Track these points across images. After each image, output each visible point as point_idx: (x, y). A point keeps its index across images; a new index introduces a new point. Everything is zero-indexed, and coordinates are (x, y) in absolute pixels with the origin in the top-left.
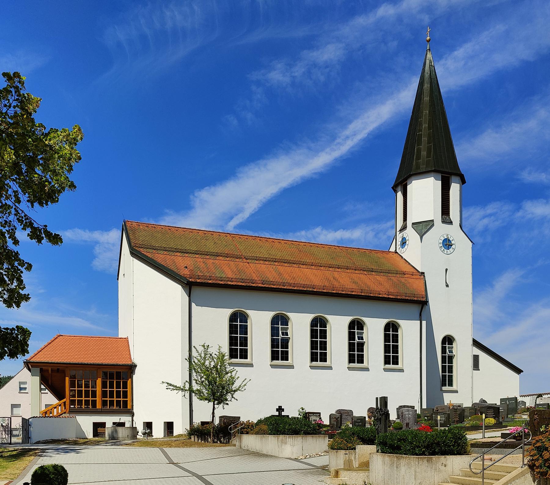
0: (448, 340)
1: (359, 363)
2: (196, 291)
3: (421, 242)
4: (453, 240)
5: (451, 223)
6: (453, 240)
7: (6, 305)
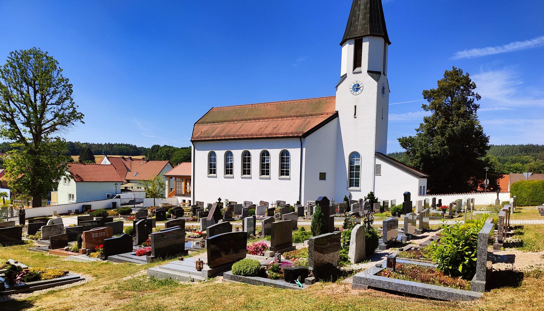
0: (355, 155)
2: (197, 144)
6: (361, 84)
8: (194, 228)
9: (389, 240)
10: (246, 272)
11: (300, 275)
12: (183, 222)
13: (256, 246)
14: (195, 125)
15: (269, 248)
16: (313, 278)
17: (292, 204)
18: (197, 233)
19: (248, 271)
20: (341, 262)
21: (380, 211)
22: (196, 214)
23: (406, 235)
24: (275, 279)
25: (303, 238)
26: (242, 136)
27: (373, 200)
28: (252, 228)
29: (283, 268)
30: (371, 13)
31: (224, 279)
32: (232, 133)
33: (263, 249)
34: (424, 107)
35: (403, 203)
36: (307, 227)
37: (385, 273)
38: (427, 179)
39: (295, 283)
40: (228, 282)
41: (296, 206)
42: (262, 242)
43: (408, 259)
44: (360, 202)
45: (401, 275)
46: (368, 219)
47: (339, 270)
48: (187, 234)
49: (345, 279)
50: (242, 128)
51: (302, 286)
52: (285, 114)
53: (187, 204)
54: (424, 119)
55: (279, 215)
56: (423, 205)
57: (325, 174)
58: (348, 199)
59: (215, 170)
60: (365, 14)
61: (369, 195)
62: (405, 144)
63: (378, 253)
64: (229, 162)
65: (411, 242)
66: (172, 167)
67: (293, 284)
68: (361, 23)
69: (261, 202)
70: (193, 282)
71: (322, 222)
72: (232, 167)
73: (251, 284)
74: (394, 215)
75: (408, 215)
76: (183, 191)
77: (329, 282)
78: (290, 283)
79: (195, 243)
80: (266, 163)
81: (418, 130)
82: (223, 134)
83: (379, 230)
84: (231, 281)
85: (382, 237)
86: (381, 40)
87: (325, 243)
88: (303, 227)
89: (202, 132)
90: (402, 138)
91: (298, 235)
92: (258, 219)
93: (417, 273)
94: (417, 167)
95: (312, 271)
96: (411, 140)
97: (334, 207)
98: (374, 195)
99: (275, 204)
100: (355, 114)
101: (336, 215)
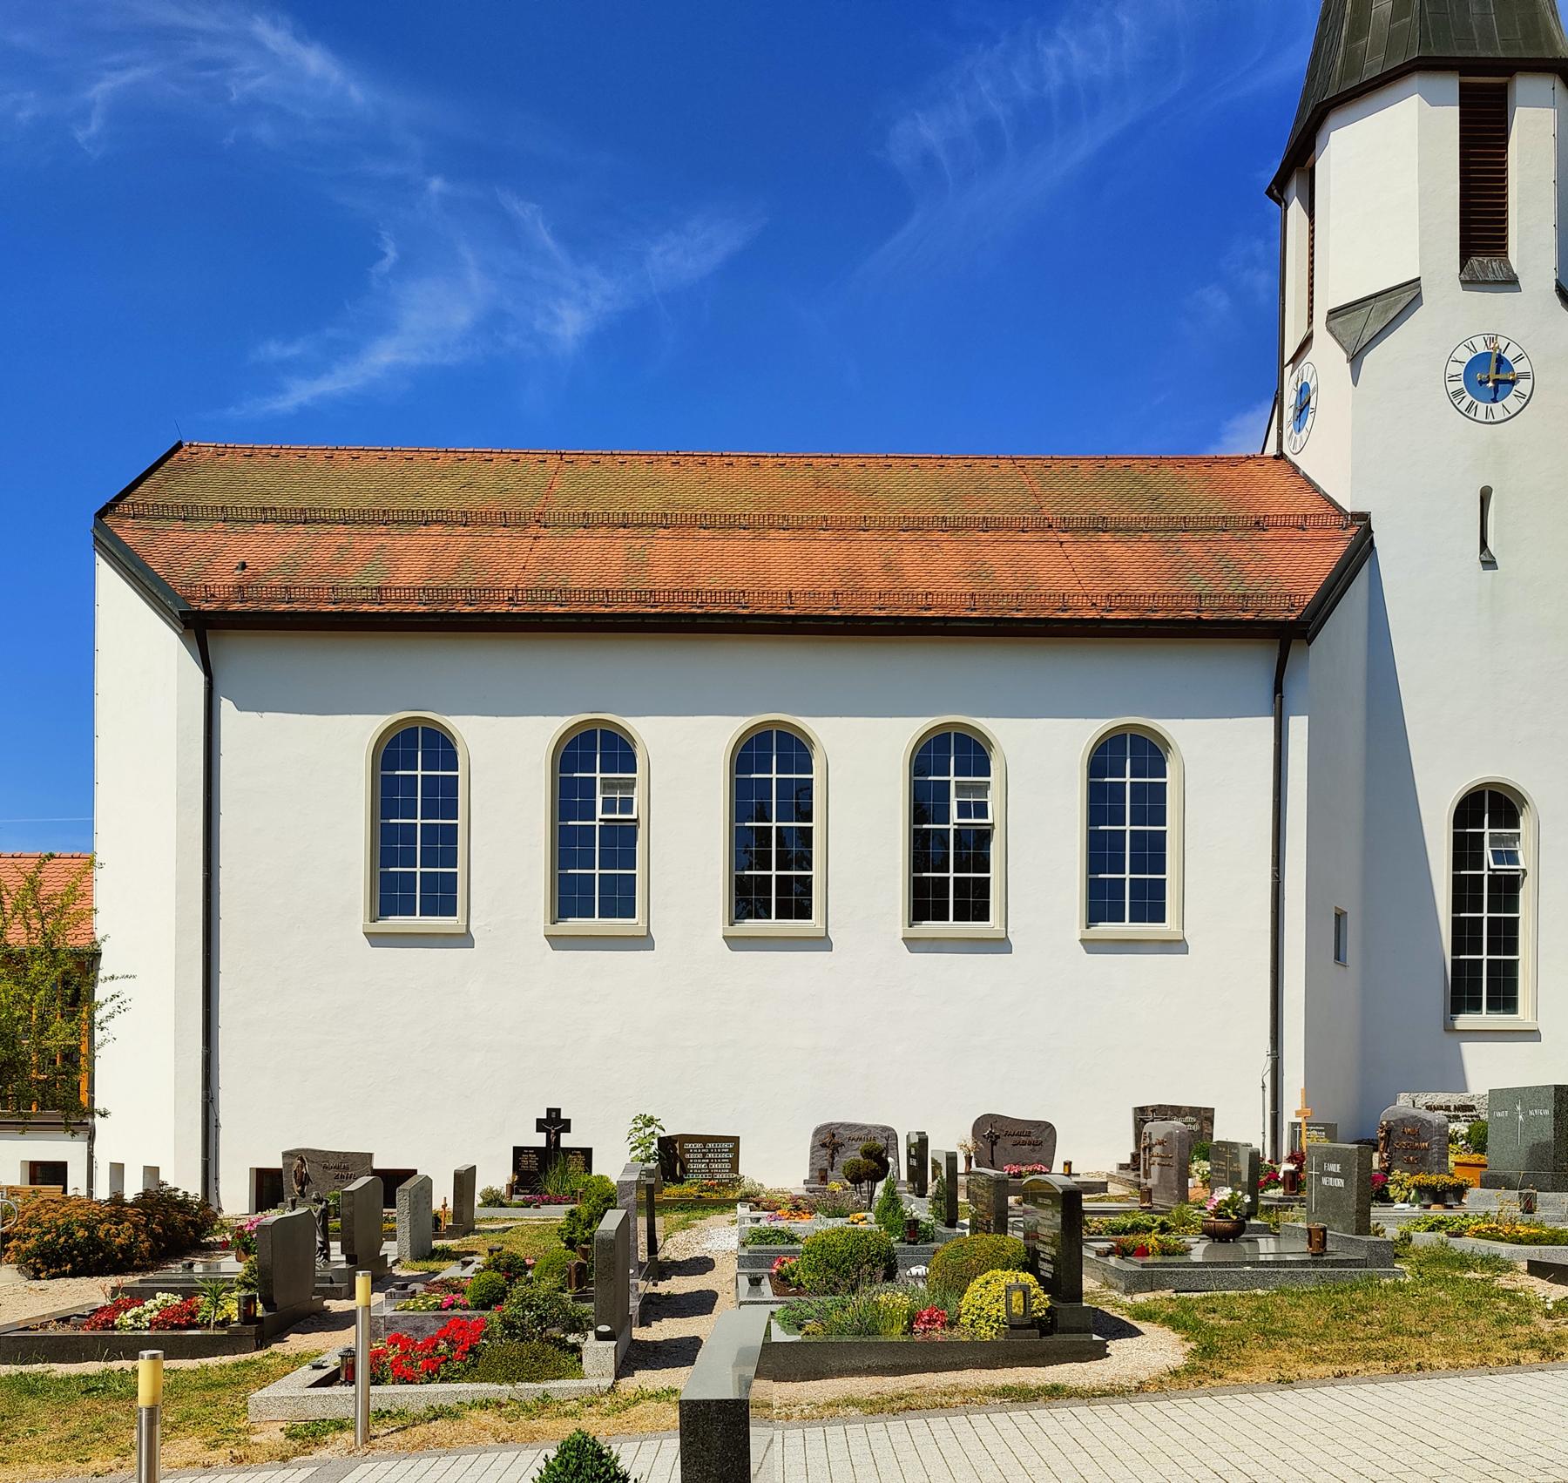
2: (235, 651)
3: (1355, 384)
4: (1519, 358)
5: (1510, 282)
6: (1519, 358)
38: (544, 1145)
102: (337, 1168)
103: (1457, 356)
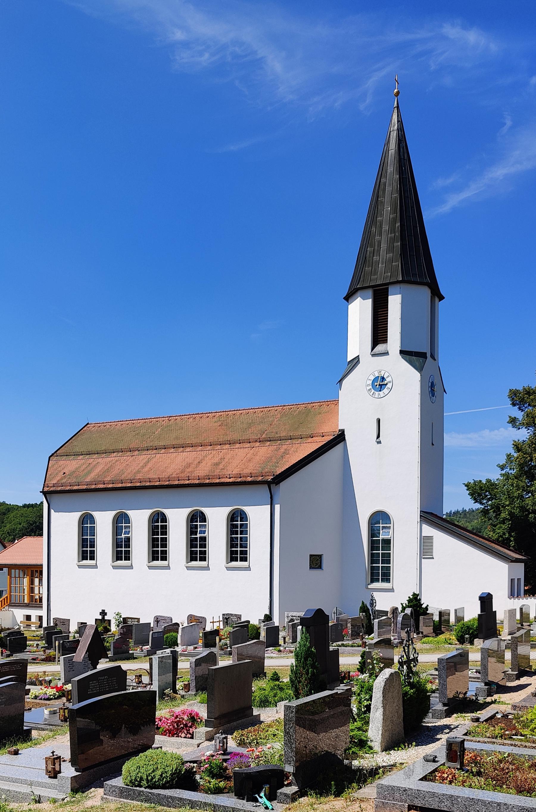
1: (163, 561)
2: (55, 498)
6: (388, 376)
7: (453, 511)
8: (47, 678)
9: (451, 696)
10: (152, 779)
11: (267, 784)
12: (24, 664)
13: (177, 717)
14: (51, 458)
15: (204, 721)
16: (294, 789)
17: (255, 621)
18: (52, 688)
19: (157, 777)
20: (353, 749)
21: (434, 631)
22: (54, 646)
23: (486, 684)
24: (214, 793)
25: (275, 696)
26: (150, 482)
27: (419, 611)
28: (169, 677)
29: (232, 767)
30: (402, 238)
31: (105, 796)
32: (127, 475)
33: (190, 724)
34: (513, 421)
35: (479, 615)
36: (286, 670)
37: (443, 775)
38: (523, 564)
39: (256, 801)
40: (114, 803)
41: (263, 624)
42: (190, 709)
43: (489, 740)
44: (393, 613)
45: (475, 779)
46: (408, 656)
47: (349, 767)
48: (32, 691)
49: (361, 788)
50: (150, 465)
51: (270, 808)
52: (236, 436)
53: (33, 623)
54: (513, 444)
55: (226, 645)
56: (518, 617)
57: (320, 556)
58: (369, 610)
59: (92, 552)
60: (392, 241)
61: (410, 601)
62: (479, 495)
63: (430, 725)
64: (123, 536)
65: (496, 700)
66: (3, 548)
67: (252, 803)
68: (383, 259)
69: (191, 618)
70: (39, 803)
71: (313, 666)
72: (128, 545)
73: (163, 806)
74: (461, 640)
75: (491, 644)
76: (26, 597)
77: (327, 796)
78: (247, 801)
79: (46, 712)
80: (198, 535)
81: (502, 467)
82: (108, 479)
83: (432, 675)
84: (121, 800)
85: (437, 689)
86: (426, 292)
87: (319, 708)
88: (275, 672)
89: (64, 473)
90: (472, 482)
91: (265, 690)
92: (182, 655)
93: (507, 773)
94: (504, 540)
95: (293, 773)
96: (491, 486)
97: (340, 627)
98: (420, 600)
99: (219, 621)
100: (378, 436)
101: (344, 643)
102: (62, 622)
103: (370, 378)
